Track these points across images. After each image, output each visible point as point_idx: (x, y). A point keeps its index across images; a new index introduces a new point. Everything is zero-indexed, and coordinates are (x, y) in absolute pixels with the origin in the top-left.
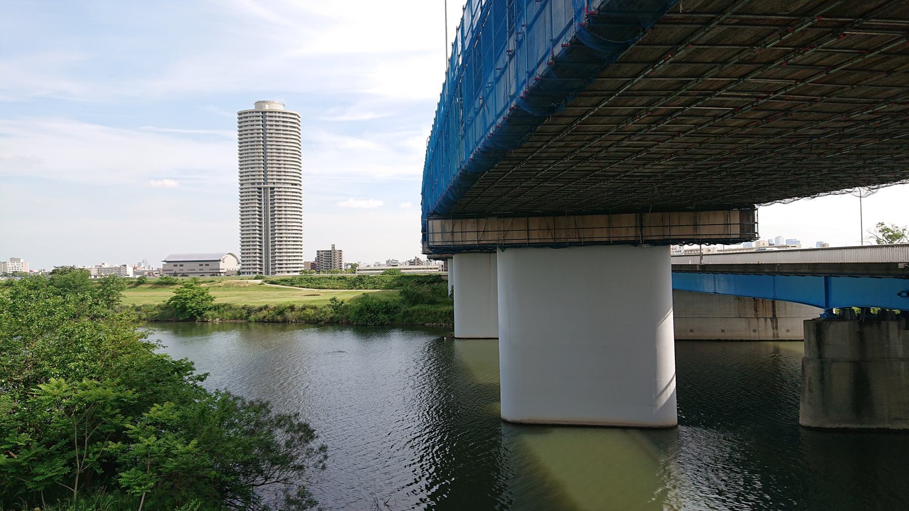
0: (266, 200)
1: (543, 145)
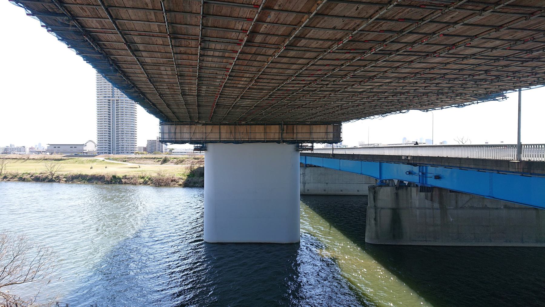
1: (303, 67)
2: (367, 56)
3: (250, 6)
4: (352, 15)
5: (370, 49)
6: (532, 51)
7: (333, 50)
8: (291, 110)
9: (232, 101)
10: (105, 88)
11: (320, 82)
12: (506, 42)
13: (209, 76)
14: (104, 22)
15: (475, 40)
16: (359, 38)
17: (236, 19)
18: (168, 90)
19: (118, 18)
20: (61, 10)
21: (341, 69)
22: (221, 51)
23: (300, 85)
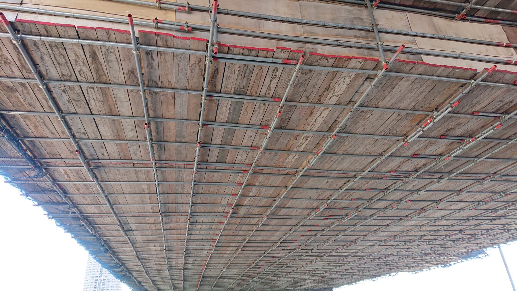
2: (344, 221)
3: (235, 184)
4: (324, 187)
5: (346, 215)
6: (496, 210)
7: (312, 217)
8: (280, 278)
9: (218, 272)
10: (94, 268)
11: (305, 247)
12: (470, 204)
13: (197, 249)
14: (102, 208)
15: (441, 203)
16: (334, 206)
17: (223, 195)
18: (155, 266)
19: (115, 203)
20: (64, 200)
21: (323, 235)
22: (209, 224)
23: (285, 251)
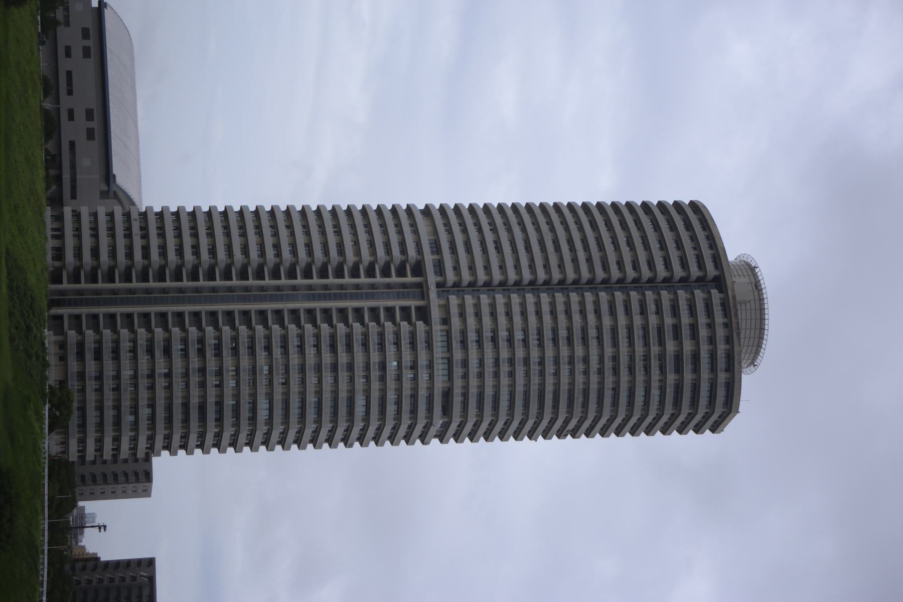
0: (373, 291)
